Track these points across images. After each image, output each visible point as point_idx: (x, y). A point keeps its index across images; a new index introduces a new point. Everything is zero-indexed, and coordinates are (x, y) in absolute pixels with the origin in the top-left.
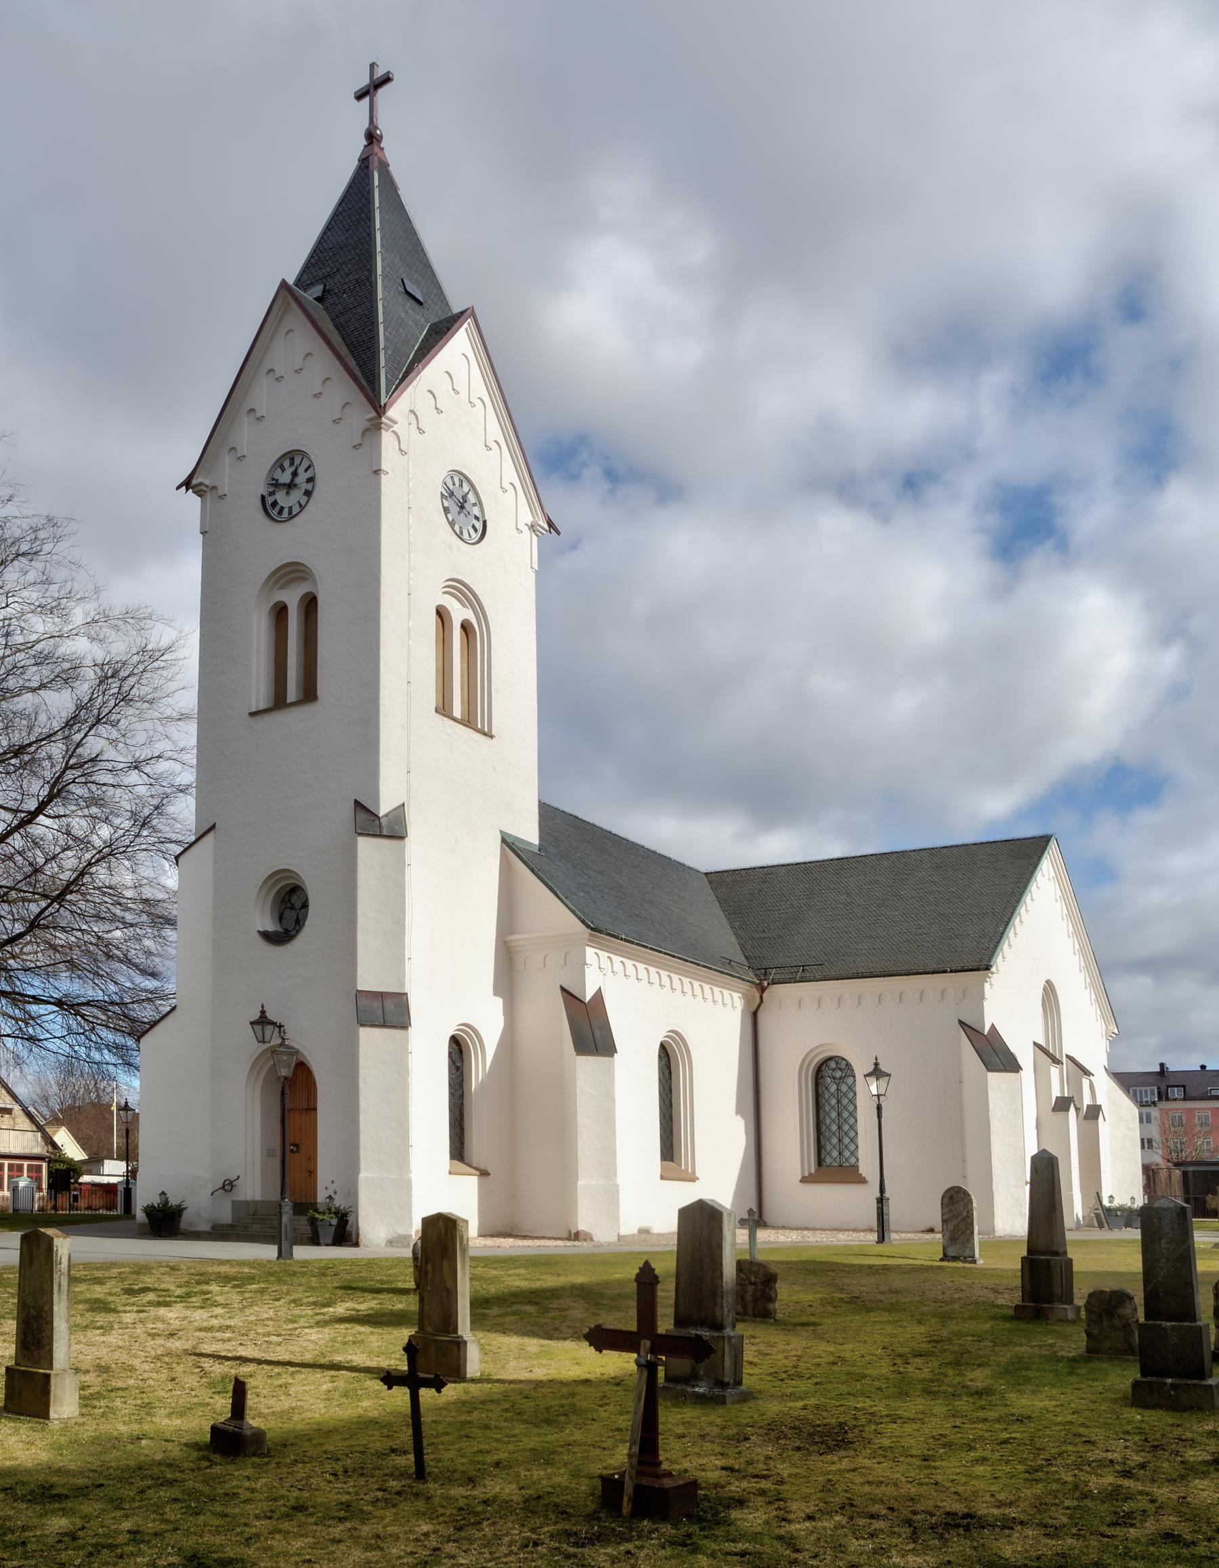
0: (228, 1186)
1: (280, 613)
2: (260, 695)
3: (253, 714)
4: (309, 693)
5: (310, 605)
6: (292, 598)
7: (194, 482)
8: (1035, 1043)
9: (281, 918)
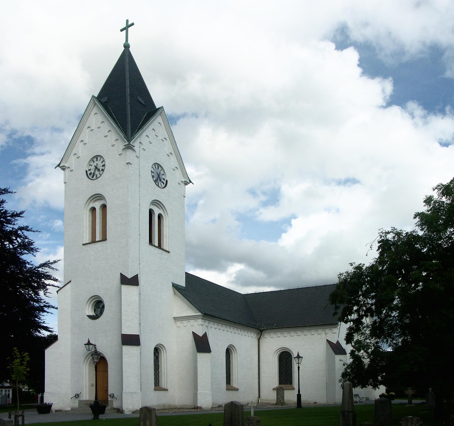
0: (77, 396)
1: (93, 210)
2: (87, 238)
3: (84, 245)
4: (104, 239)
5: (104, 207)
6: (98, 205)
7: (61, 165)
8: (327, 340)
9: (95, 311)
